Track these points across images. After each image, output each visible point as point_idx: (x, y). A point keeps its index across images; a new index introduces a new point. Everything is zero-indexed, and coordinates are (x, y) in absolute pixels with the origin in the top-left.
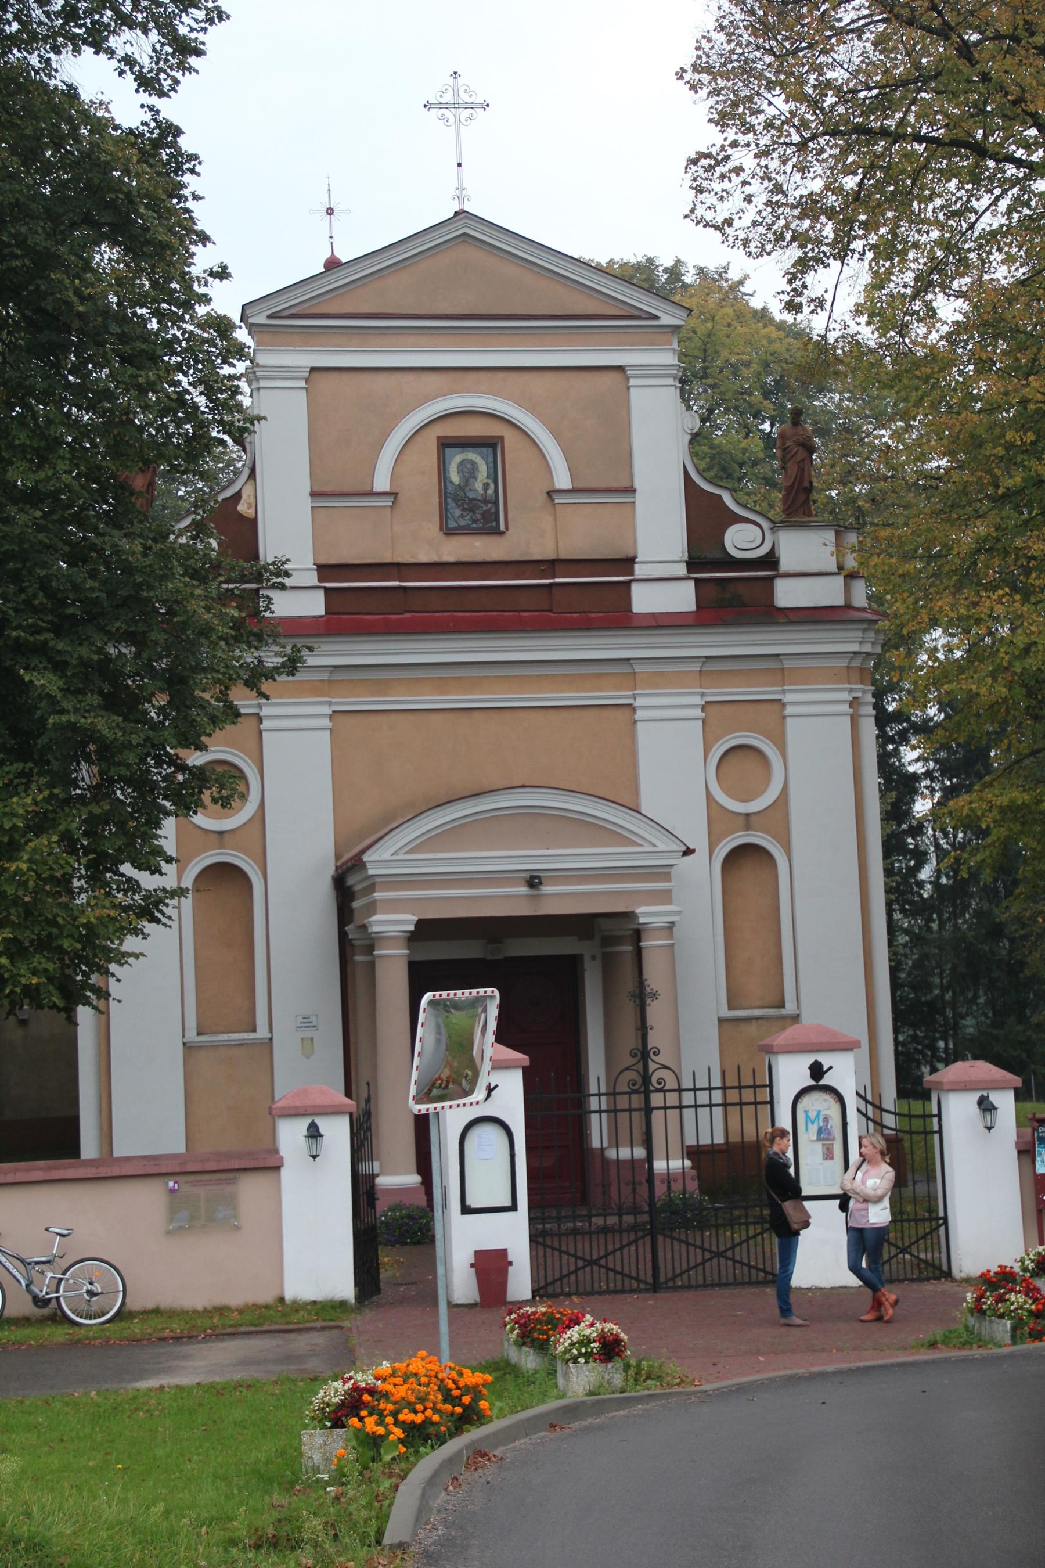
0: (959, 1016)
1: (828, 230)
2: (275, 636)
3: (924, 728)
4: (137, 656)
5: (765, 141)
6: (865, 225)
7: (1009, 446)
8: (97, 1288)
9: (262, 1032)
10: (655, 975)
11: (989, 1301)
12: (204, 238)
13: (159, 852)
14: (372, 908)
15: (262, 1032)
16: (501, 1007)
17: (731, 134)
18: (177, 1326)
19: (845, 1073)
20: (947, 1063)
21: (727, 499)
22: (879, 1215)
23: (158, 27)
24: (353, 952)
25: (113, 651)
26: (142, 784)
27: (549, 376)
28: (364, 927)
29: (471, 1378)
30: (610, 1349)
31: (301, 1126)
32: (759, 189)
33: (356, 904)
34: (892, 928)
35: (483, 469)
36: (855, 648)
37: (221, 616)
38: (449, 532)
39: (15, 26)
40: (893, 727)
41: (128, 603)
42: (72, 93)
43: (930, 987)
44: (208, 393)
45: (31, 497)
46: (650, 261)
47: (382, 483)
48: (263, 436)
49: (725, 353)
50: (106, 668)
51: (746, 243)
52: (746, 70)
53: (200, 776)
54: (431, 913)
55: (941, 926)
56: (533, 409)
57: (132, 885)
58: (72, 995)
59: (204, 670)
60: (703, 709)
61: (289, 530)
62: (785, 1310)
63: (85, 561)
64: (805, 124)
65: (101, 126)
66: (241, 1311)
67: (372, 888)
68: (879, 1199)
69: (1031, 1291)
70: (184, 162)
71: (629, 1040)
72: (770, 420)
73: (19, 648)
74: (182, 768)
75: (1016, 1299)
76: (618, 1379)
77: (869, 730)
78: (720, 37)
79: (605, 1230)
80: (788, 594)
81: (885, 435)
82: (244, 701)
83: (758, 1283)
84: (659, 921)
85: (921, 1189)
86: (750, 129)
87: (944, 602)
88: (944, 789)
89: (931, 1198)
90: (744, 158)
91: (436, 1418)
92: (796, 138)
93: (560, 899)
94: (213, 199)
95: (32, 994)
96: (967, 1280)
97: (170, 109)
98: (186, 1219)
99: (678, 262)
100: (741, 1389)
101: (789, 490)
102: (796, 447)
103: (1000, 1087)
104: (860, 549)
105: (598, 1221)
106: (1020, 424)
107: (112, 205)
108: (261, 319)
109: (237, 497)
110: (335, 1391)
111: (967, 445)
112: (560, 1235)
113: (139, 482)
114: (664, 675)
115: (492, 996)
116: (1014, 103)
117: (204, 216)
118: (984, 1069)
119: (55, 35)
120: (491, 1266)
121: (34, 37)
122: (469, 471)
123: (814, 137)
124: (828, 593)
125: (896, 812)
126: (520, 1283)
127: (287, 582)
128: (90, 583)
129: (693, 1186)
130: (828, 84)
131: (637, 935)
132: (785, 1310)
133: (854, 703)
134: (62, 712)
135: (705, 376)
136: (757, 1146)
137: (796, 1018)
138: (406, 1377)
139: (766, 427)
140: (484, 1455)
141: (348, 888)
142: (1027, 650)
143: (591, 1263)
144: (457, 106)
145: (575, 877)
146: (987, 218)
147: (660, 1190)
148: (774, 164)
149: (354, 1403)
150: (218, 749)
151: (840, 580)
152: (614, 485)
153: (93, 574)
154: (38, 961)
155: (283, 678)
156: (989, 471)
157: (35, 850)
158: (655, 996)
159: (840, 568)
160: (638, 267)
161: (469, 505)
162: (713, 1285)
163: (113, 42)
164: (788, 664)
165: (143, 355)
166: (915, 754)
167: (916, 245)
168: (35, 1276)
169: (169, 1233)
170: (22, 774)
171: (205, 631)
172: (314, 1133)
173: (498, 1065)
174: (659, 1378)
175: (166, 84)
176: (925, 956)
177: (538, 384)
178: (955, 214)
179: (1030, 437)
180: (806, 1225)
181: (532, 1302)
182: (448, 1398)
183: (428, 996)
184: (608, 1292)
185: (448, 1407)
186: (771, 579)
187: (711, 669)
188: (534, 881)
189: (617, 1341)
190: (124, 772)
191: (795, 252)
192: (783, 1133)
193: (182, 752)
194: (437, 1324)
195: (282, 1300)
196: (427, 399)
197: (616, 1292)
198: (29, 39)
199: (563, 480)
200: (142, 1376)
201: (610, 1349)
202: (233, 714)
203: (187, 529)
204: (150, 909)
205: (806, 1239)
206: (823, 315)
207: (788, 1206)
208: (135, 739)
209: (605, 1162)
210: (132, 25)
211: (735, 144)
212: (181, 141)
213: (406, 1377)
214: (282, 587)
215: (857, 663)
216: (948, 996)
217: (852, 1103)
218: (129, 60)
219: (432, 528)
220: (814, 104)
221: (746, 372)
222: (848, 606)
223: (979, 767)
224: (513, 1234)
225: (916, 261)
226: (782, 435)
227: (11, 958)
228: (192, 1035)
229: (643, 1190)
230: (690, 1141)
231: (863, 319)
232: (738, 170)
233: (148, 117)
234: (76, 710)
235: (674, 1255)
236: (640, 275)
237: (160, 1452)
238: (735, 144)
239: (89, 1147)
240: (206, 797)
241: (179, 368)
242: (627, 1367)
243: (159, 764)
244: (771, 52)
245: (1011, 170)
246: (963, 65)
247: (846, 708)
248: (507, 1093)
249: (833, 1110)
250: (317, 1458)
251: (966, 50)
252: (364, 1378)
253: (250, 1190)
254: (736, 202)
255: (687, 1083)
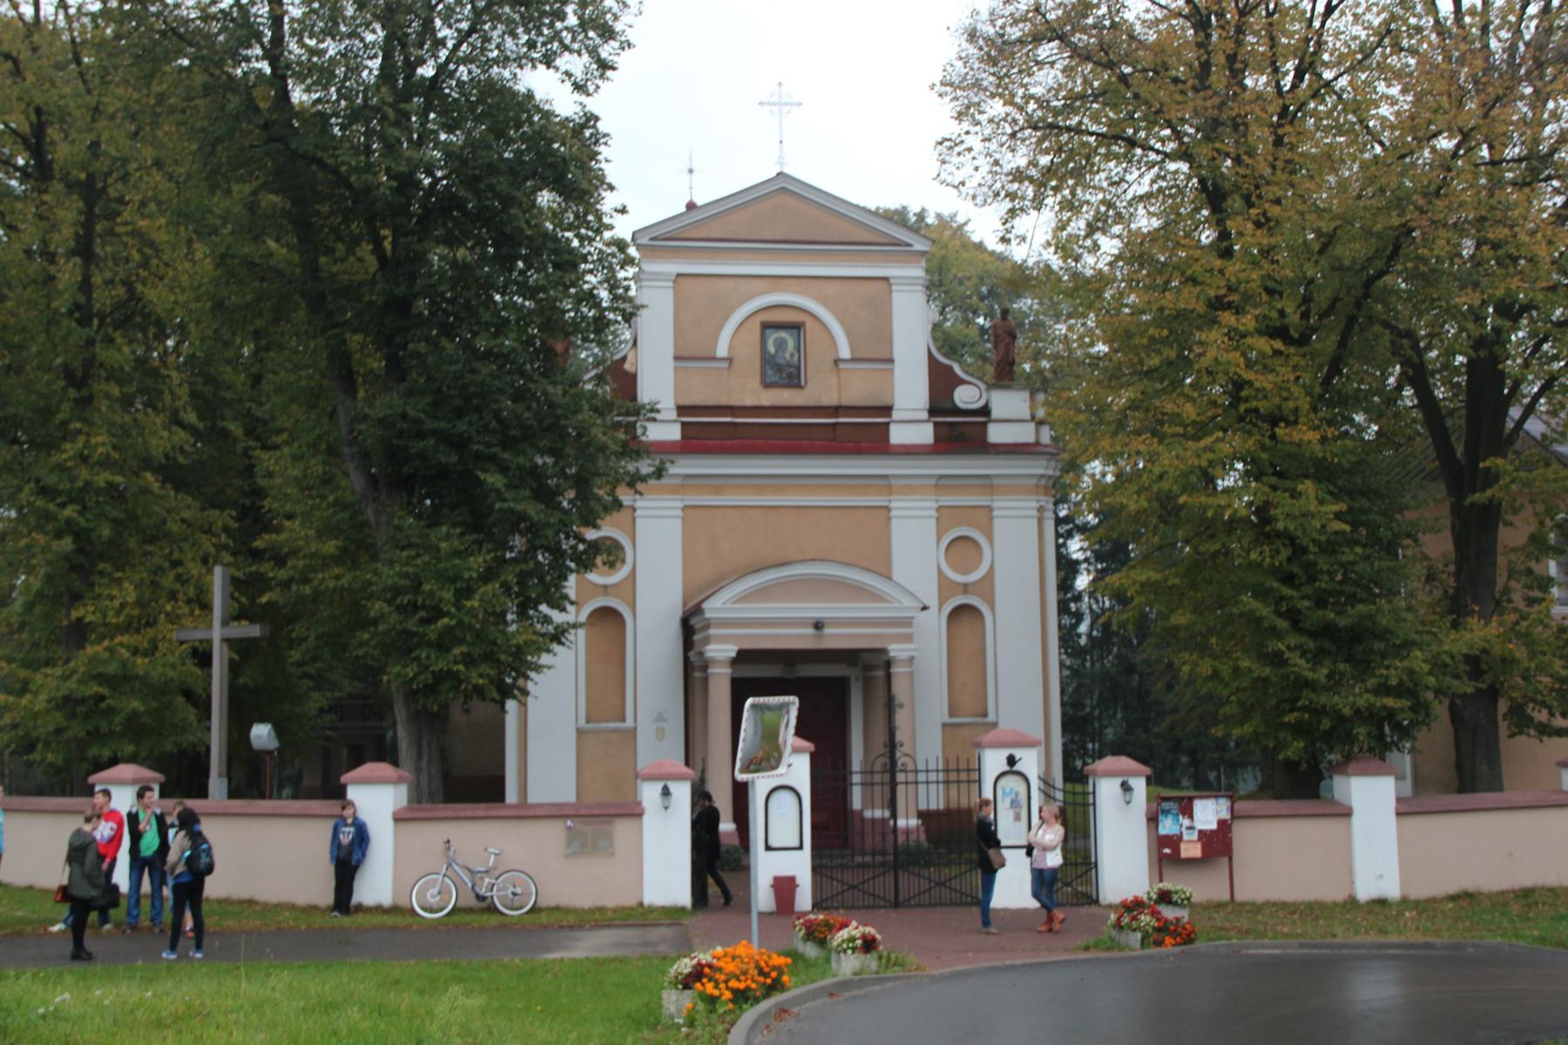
0: (1102, 727)
1: (1030, 192)
2: (648, 453)
3: (1083, 529)
4: (555, 464)
5: (987, 132)
6: (1053, 188)
7: (1152, 339)
8: (518, 890)
9: (629, 723)
10: (900, 689)
11: (1125, 920)
12: (611, 188)
13: (566, 597)
14: (707, 640)
15: (629, 723)
16: (800, 710)
17: (966, 126)
18: (571, 919)
19: (1030, 762)
20: (1100, 757)
21: (957, 369)
22: (1054, 859)
23: (589, 52)
24: (693, 670)
25: (540, 461)
26: (557, 553)
27: (837, 284)
28: (701, 654)
29: (778, 960)
30: (869, 945)
31: (658, 786)
32: (984, 164)
33: (696, 637)
34: (1062, 665)
35: (791, 343)
36: (1042, 471)
37: (614, 439)
38: (767, 385)
39: (496, 53)
40: (1067, 527)
41: (551, 429)
42: (530, 96)
43: (1083, 706)
44: (611, 290)
45: (489, 355)
46: (904, 208)
47: (722, 351)
48: (643, 320)
49: (954, 270)
50: (534, 472)
51: (974, 197)
52: (977, 85)
53: (595, 547)
54: (748, 645)
55: (1093, 664)
56: (826, 304)
57: (547, 620)
58: (506, 692)
59: (601, 475)
60: (938, 510)
61: (658, 382)
62: (986, 922)
63: (524, 400)
64: (1015, 121)
65: (548, 115)
66: (614, 910)
67: (707, 627)
68: (1053, 849)
69: (1155, 913)
70: (597, 138)
71: (880, 738)
72: (988, 315)
73: (478, 456)
74: (583, 541)
75: (1145, 919)
76: (874, 965)
77: (1050, 526)
78: (959, 64)
79: (863, 865)
80: (996, 434)
81: (1061, 328)
82: (625, 496)
83: (966, 904)
84: (903, 655)
85: (1080, 843)
86: (978, 123)
87: (1105, 443)
88: (1097, 571)
89: (1087, 850)
90: (974, 141)
91: (754, 986)
92: (1009, 131)
93: (835, 638)
94: (614, 161)
95: (479, 691)
96: (1110, 906)
97: (593, 104)
98: (579, 847)
99: (923, 210)
100: (958, 975)
101: (999, 364)
102: (1005, 333)
103: (1135, 774)
104: (1046, 404)
105: (858, 859)
106: (1156, 323)
107: (552, 166)
108: (644, 241)
109: (624, 359)
110: (685, 965)
111: (1121, 337)
112: (832, 868)
113: (559, 347)
114: (910, 487)
115: (793, 701)
116: (1156, 113)
117: (611, 173)
118: (1124, 762)
119: (520, 58)
120: (784, 887)
121: (507, 58)
122: (780, 344)
123: (1022, 129)
124: (1024, 434)
125: (1065, 585)
126: (804, 899)
127: (658, 416)
128: (526, 415)
129: (923, 837)
130: (1032, 97)
131: (888, 664)
132: (986, 922)
133: (1041, 509)
134: (505, 500)
135: (941, 285)
136: (969, 811)
137: (995, 725)
138: (734, 958)
139: (981, 320)
140: (785, 1011)
141: (690, 627)
142: (1161, 477)
143: (853, 887)
144: (780, 104)
145: (846, 623)
146: (1134, 187)
147: (901, 839)
148: (993, 146)
149: (698, 974)
150: (607, 529)
151: (1032, 426)
152: (880, 356)
153: (529, 408)
154: (484, 668)
155: (652, 482)
156: (1138, 354)
157: (484, 594)
158: (901, 706)
159: (1033, 417)
160: (896, 212)
161: (779, 369)
162: (936, 905)
163: (558, 62)
164: (996, 481)
165: (569, 262)
166: (1078, 546)
167: (1088, 202)
168: (478, 881)
169: (567, 856)
170: (476, 542)
171: (603, 448)
172: (666, 792)
173: (796, 750)
174: (902, 965)
175: (591, 88)
176: (1080, 686)
177: (830, 288)
178: (1112, 184)
179: (1165, 332)
180: (1003, 865)
181: (812, 911)
182: (761, 972)
183: (750, 701)
184: (864, 907)
185: (762, 979)
186: (985, 424)
187: (943, 484)
188: (818, 625)
189: (874, 940)
190: (544, 542)
191: (1007, 205)
192: (987, 803)
193: (582, 530)
194: (749, 925)
195: (641, 904)
196: (763, 293)
197: (869, 907)
198: (504, 61)
199: (845, 353)
200: (549, 950)
201: (869, 945)
202: (618, 505)
203: (591, 379)
204: (558, 636)
205: (1001, 875)
206: (1025, 246)
207: (992, 852)
208: (552, 520)
209: (863, 819)
210: (571, 51)
211: (967, 133)
212: (599, 124)
213: (734, 958)
214: (654, 420)
215: (1043, 482)
216: (1096, 713)
217: (1035, 784)
218: (568, 74)
219: (755, 382)
220: (1021, 109)
221: (968, 283)
222: (1037, 443)
223: (1121, 556)
224: (800, 865)
225: (1088, 214)
226: (994, 327)
227: (466, 665)
228: (582, 722)
229: (890, 839)
230: (923, 806)
231: (1052, 249)
232: (970, 150)
233: (578, 109)
234: (514, 500)
235: (910, 883)
236: (898, 217)
237: (564, 1001)
238: (967, 133)
239: (511, 796)
240: (599, 561)
241: (591, 272)
242: (880, 958)
243: (567, 538)
244: (994, 74)
245: (1153, 156)
246: (1122, 87)
247: (1034, 513)
248: (797, 769)
249: (1022, 788)
250: (673, 1009)
251: (1123, 79)
252: (705, 958)
253: (621, 828)
254: (968, 169)
255: (921, 766)
